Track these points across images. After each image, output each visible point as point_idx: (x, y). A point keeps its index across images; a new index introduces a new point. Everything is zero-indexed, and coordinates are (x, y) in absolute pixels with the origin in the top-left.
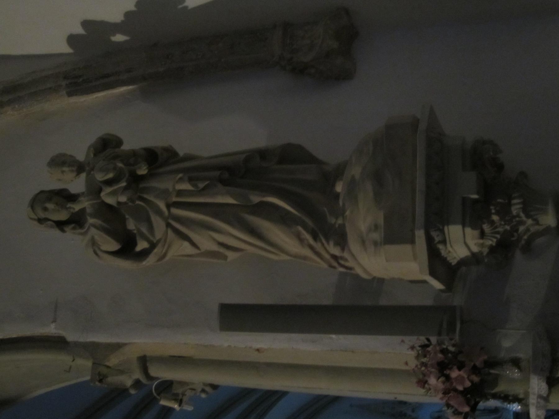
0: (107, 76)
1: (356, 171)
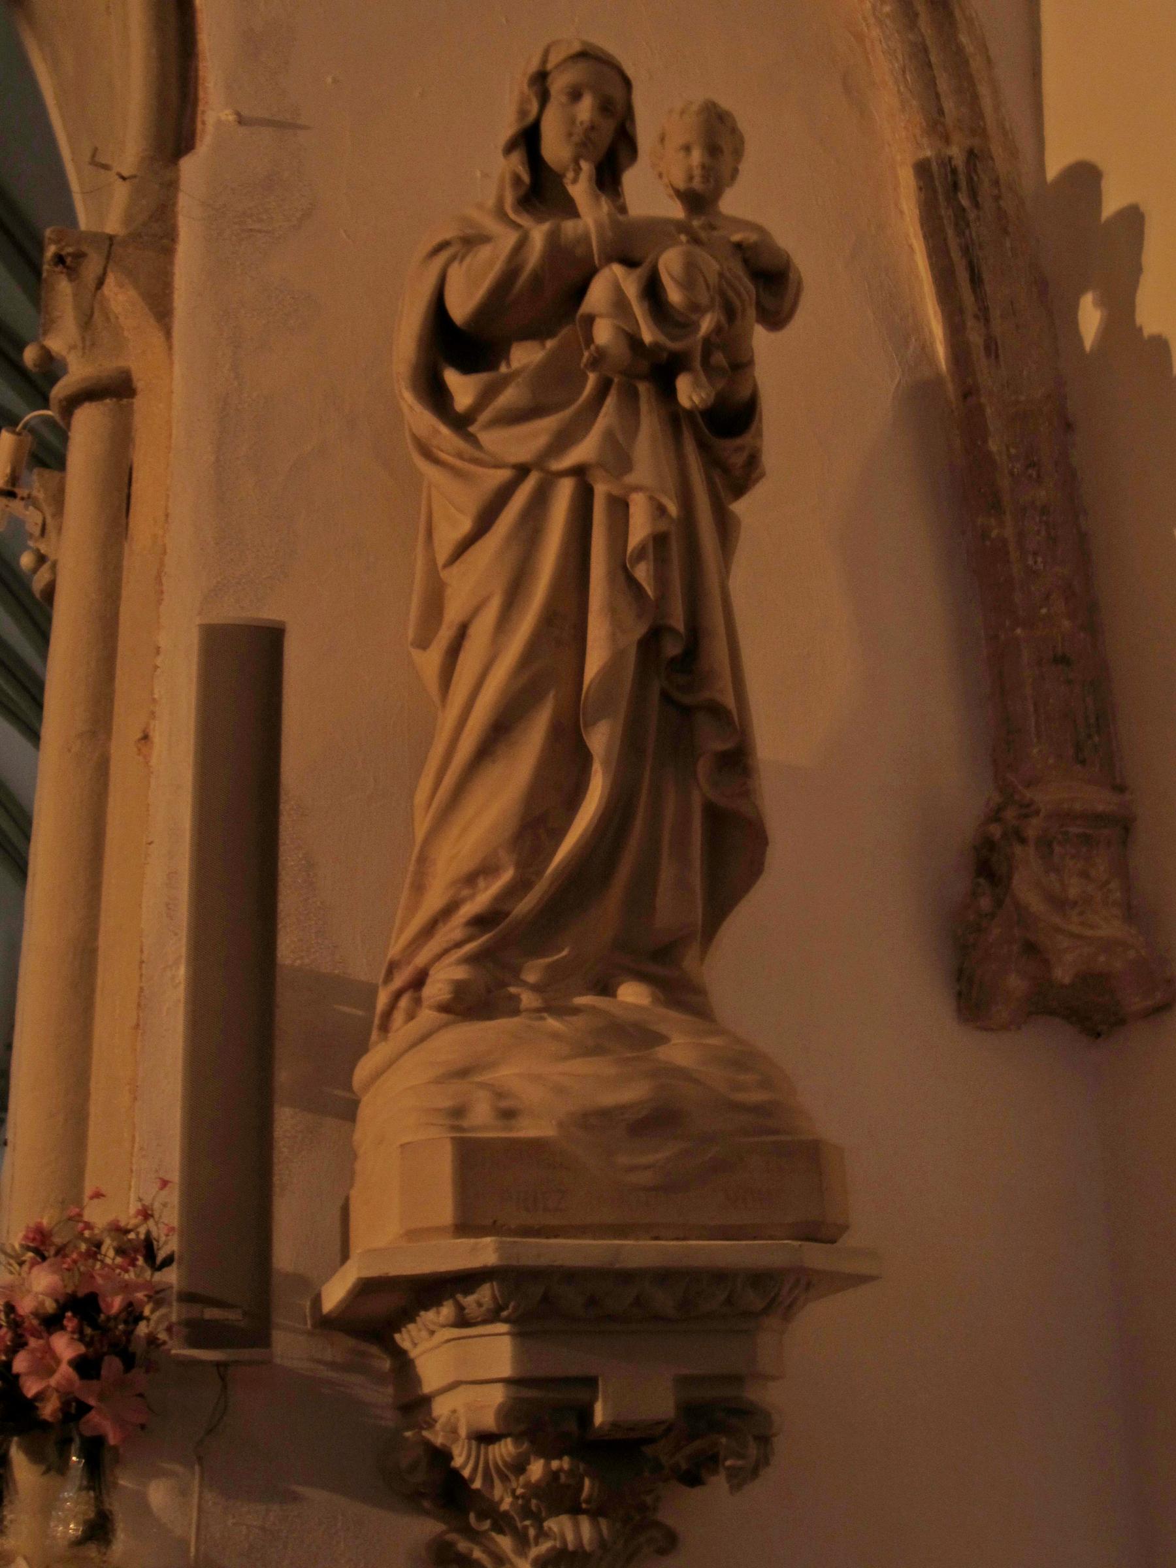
0: (976, 280)
1: (681, 1049)
